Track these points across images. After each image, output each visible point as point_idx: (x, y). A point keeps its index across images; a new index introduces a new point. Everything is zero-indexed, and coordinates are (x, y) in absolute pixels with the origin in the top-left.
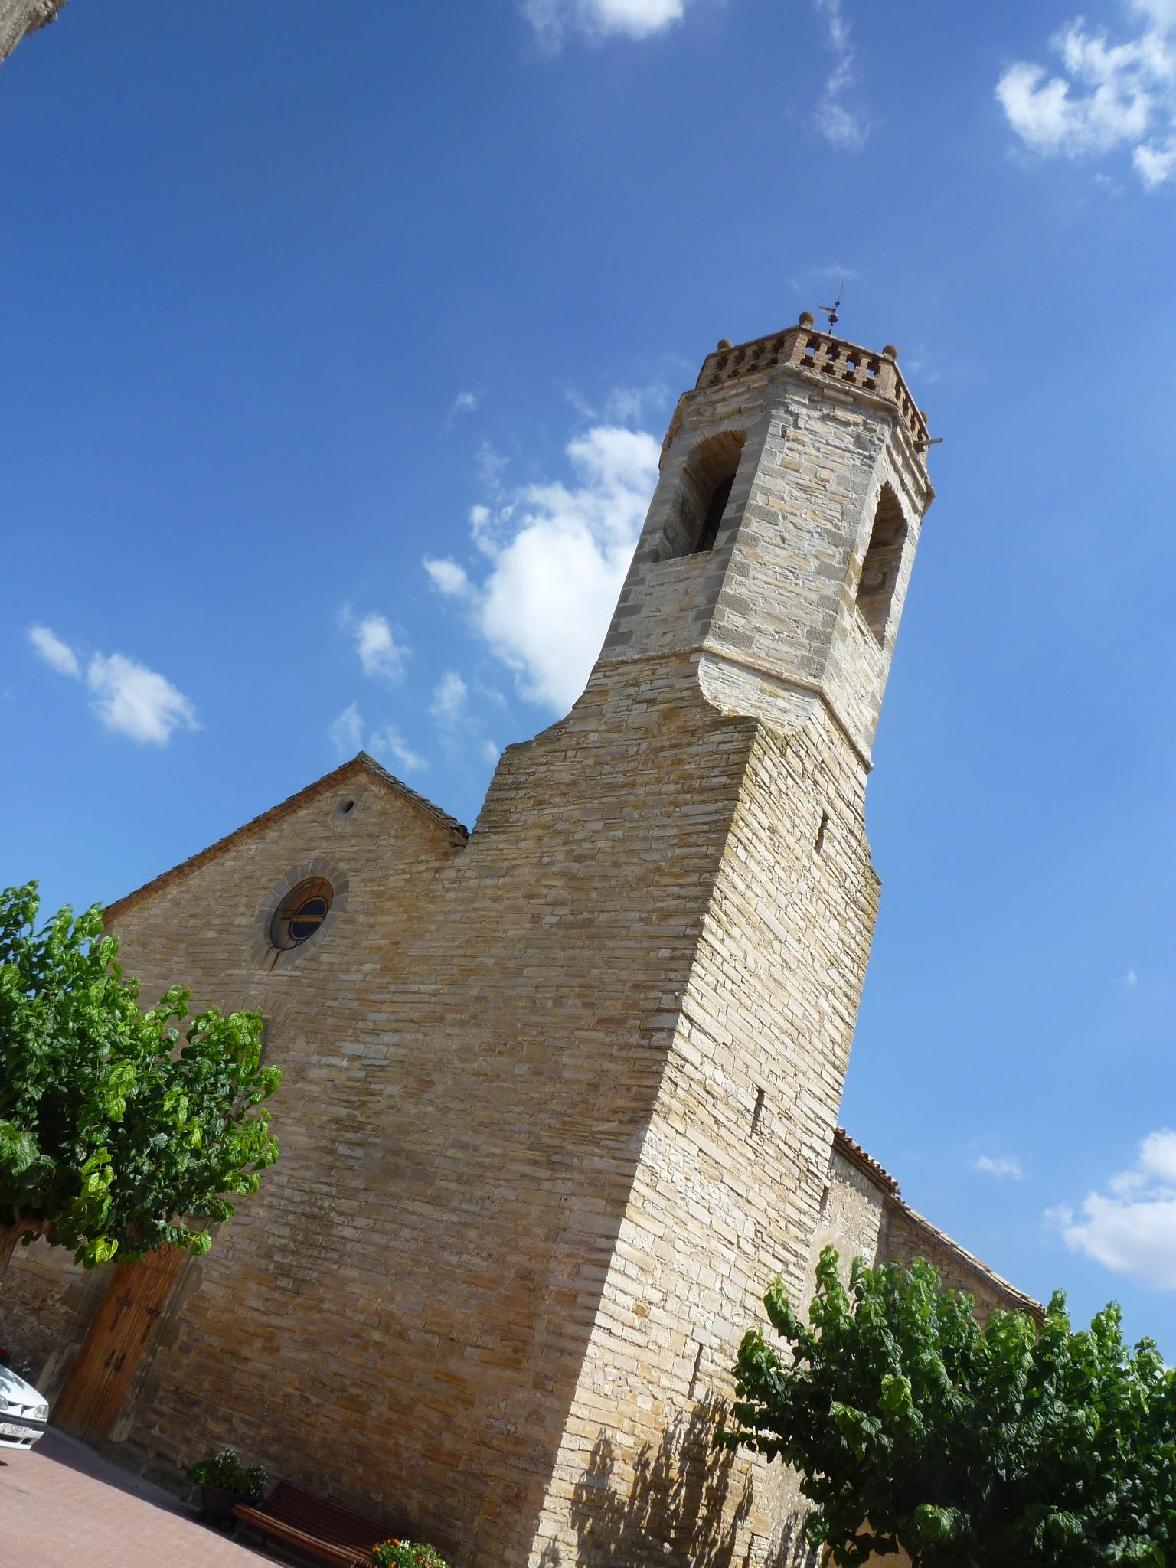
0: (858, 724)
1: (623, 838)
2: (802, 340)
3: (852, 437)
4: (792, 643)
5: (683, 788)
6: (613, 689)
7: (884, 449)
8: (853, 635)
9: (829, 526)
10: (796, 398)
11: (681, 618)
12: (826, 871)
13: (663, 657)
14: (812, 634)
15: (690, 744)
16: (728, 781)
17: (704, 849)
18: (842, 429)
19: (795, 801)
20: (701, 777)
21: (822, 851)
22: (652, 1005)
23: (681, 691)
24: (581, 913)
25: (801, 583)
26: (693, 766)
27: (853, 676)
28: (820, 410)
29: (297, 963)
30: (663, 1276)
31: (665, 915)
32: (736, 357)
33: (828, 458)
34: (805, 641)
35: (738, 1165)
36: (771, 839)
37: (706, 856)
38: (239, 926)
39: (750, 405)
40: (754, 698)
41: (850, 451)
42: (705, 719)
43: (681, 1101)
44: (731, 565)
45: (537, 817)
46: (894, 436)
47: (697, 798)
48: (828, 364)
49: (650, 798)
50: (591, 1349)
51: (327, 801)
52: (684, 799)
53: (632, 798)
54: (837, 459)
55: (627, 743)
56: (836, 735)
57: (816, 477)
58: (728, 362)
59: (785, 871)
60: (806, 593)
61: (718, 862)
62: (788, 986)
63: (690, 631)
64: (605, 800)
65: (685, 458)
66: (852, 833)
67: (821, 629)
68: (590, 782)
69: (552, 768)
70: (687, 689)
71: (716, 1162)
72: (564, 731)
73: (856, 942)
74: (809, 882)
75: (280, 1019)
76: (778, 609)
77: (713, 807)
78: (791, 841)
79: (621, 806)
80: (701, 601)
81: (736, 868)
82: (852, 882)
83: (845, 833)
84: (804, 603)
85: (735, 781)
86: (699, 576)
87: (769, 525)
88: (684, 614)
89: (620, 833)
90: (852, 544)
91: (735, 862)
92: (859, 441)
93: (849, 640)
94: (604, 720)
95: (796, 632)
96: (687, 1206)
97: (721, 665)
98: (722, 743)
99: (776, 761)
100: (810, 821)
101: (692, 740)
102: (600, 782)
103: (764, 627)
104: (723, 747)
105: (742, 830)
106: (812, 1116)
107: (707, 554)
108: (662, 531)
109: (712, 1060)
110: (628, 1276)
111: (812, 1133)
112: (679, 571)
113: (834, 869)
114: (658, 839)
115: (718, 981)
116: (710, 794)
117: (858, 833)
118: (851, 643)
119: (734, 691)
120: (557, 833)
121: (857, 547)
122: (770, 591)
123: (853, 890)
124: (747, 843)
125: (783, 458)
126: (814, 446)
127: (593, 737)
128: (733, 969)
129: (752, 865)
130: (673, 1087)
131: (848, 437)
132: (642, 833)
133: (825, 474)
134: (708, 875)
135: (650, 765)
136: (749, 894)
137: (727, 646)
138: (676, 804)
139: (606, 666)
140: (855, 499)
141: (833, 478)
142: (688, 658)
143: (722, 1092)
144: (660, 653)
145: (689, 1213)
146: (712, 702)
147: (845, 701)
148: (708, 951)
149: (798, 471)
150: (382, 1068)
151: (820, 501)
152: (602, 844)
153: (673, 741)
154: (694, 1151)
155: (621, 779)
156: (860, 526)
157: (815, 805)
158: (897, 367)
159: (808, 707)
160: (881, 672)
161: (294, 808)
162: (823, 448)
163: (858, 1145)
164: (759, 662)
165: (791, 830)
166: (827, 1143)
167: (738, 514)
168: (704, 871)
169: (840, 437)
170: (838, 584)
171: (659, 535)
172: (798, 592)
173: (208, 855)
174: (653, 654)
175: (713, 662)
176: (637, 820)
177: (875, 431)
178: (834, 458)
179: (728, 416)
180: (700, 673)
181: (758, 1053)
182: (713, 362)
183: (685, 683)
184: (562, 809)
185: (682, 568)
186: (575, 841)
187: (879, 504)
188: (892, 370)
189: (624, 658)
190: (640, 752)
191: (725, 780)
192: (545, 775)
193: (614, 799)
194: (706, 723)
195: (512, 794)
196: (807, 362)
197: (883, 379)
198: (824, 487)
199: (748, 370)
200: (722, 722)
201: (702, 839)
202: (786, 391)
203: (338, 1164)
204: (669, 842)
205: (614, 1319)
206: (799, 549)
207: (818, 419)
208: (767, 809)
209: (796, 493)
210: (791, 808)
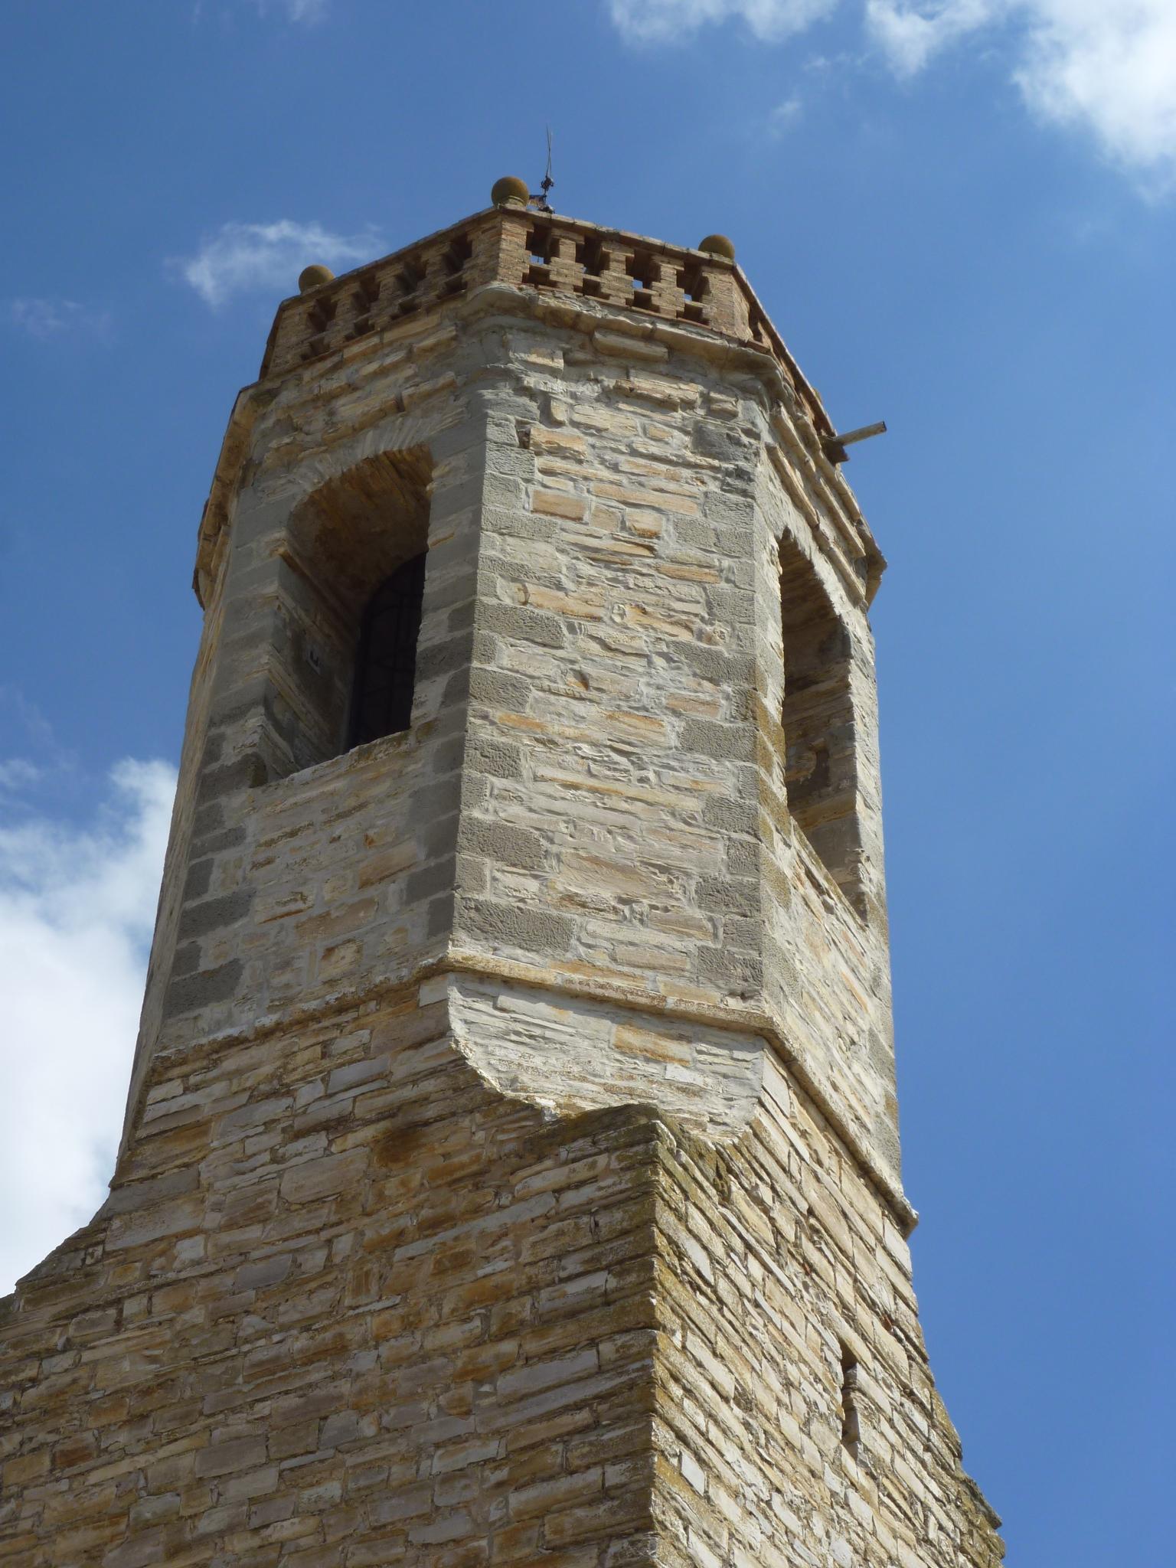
0: (861, 1112)
1: (346, 1500)
2: (513, 240)
3: (687, 433)
4: (667, 922)
5: (486, 1330)
6: (218, 1116)
7: (764, 455)
8: (801, 890)
9: (685, 636)
10: (533, 358)
11: (368, 903)
12: (881, 1503)
13: (341, 1008)
14: (711, 893)
15: (477, 1211)
16: (613, 1283)
17: (594, 1474)
18: (658, 416)
19: (777, 1318)
20: (533, 1288)
21: (860, 1447)
23: (414, 1083)
25: (652, 776)
26: (500, 1265)
27: (824, 991)
28: (597, 381)
32: (356, 296)
33: (641, 484)
34: (699, 914)
36: (747, 1426)
37: (605, 1493)
39: (425, 387)
40: (609, 1071)
41: (688, 465)
42: (501, 1137)
44: (470, 753)
45: (70, 1497)
46: (776, 425)
47: (532, 1346)
48: (585, 281)
49: (397, 1374)
52: (497, 1356)
53: (345, 1387)
55: (293, 1244)
56: (822, 1143)
57: (624, 528)
58: (339, 310)
59: (796, 1511)
60: (672, 798)
61: (647, 1503)
63: (401, 930)
64: (263, 1408)
65: (281, 534)
66: (910, 1395)
67: (728, 878)
68: (210, 1370)
69: (87, 1356)
70: (433, 1073)
72: (99, 1251)
74: (854, 1536)
76: (611, 846)
77: (587, 1359)
78: (790, 1426)
79: (317, 1413)
80: (411, 851)
81: (690, 1514)
82: (941, 1528)
83: (897, 1395)
85: (632, 1278)
86: (392, 795)
87: (540, 650)
88: (371, 892)
89: (333, 1489)
90: (750, 672)
91: (684, 1498)
92: (702, 441)
93: (796, 901)
94: (211, 1198)
95: (670, 896)
97: (504, 1000)
98: (568, 1187)
99: (715, 1214)
100: (820, 1368)
101: (478, 1198)
102: (238, 1362)
103: (588, 891)
104: (571, 1198)
105: (680, 1406)
107: (399, 741)
108: (261, 710)
112: (333, 793)
113: (896, 1495)
114: (448, 1478)
116: (572, 1327)
117: (923, 1394)
118: (801, 910)
119: (556, 1061)
120: (144, 1529)
121: (763, 680)
122: (581, 806)
123: (946, 1546)
124: (700, 1442)
125: (537, 492)
126: (603, 462)
127: (189, 1250)
129: (723, 1501)
131: (676, 433)
132: (399, 1472)
133: (645, 520)
134: (625, 1543)
135: (374, 1288)
137: (507, 950)
138: (478, 1375)
139: (184, 1062)
140: (730, 569)
141: (666, 528)
142: (414, 995)
144: (331, 998)
146: (510, 1094)
147: (820, 1054)
149: (579, 519)
151: (648, 582)
152: (287, 1529)
153: (426, 1213)
155: (300, 1343)
157: (819, 1327)
158: (744, 277)
159: (749, 1074)
160: (876, 981)
162: (625, 463)
164: (601, 980)
165: (785, 1399)
167: (458, 634)
168: (611, 1537)
169: (658, 434)
170: (742, 769)
171: (255, 720)
172: (650, 798)
174: (313, 1005)
175: (483, 995)
176: (376, 1441)
177: (734, 415)
179: (373, 421)
180: (458, 1028)
182: (298, 317)
183: (420, 1061)
184: (141, 1461)
185: (339, 785)
186: (203, 1540)
188: (735, 285)
189: (233, 1032)
190: (337, 1260)
191: (600, 1281)
192: (68, 1378)
193: (293, 1401)
194: (509, 1147)
197: (720, 304)
198: (651, 549)
199: (394, 317)
200: (552, 1135)
201: (579, 1450)
202: (505, 345)
204: (484, 1480)
206: (628, 698)
207: (598, 400)
208: (721, 1345)
209: (586, 569)
210: (773, 1338)
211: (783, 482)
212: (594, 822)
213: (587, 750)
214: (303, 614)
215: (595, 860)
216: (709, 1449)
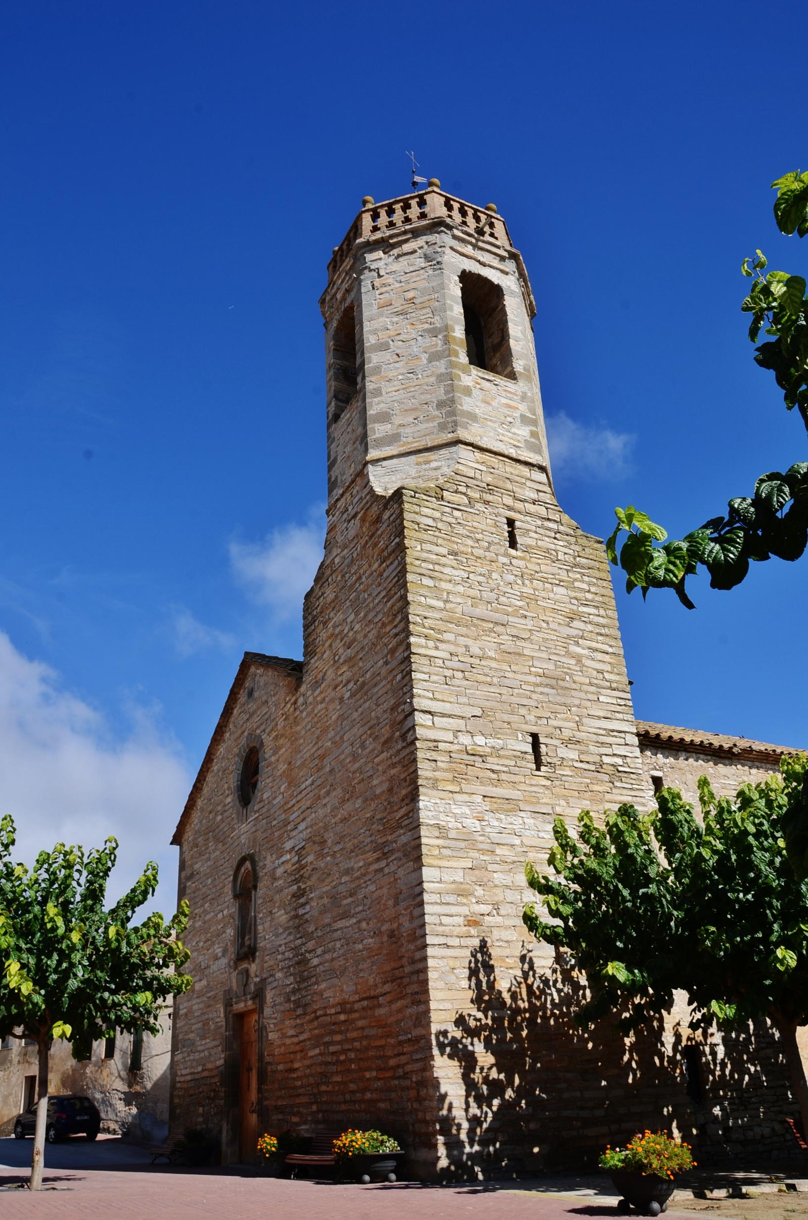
22: (401, 717)
24: (358, 681)
29: (256, 808)
30: (485, 893)
31: (393, 651)
35: (533, 794)
38: (229, 803)
43: (446, 770)
44: (368, 394)
50: (431, 962)
51: (242, 697)
54: (415, 280)
60: (427, 380)
62: (526, 652)
71: (507, 799)
73: (593, 593)
75: (257, 850)
76: (410, 404)
83: (539, 523)
84: (427, 388)
90: (447, 328)
92: (427, 258)
96: (489, 839)
99: (435, 506)
104: (391, 519)
106: (603, 732)
109: (467, 732)
110: (448, 904)
111: (611, 745)
115: (446, 677)
127: (337, 560)
128: (458, 663)
130: (433, 764)
133: (410, 295)
136: (449, 606)
137: (383, 449)
143: (489, 750)
145: (493, 843)
148: (425, 661)
150: (303, 848)
151: (413, 314)
154: (479, 799)
156: (448, 313)
161: (230, 711)
163: (700, 739)
166: (632, 745)
173: (204, 770)
178: (413, 280)
180: (371, 478)
181: (516, 710)
187: (462, 289)
195: (313, 627)
196: (375, 229)
203: (301, 921)
205: (447, 936)
209: (395, 319)
211: (460, 254)
212: (404, 399)
213: (400, 377)
214: (345, 363)
215: (406, 410)
216: (436, 574)
